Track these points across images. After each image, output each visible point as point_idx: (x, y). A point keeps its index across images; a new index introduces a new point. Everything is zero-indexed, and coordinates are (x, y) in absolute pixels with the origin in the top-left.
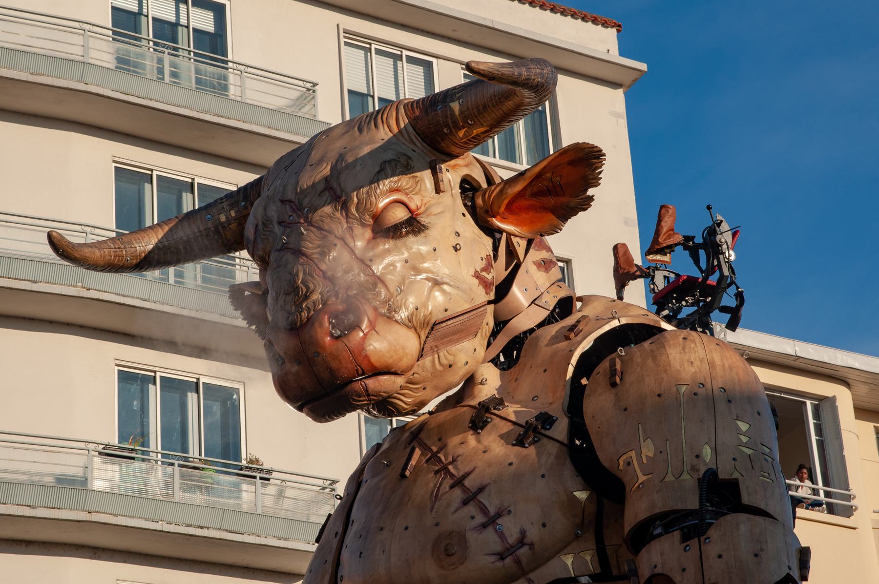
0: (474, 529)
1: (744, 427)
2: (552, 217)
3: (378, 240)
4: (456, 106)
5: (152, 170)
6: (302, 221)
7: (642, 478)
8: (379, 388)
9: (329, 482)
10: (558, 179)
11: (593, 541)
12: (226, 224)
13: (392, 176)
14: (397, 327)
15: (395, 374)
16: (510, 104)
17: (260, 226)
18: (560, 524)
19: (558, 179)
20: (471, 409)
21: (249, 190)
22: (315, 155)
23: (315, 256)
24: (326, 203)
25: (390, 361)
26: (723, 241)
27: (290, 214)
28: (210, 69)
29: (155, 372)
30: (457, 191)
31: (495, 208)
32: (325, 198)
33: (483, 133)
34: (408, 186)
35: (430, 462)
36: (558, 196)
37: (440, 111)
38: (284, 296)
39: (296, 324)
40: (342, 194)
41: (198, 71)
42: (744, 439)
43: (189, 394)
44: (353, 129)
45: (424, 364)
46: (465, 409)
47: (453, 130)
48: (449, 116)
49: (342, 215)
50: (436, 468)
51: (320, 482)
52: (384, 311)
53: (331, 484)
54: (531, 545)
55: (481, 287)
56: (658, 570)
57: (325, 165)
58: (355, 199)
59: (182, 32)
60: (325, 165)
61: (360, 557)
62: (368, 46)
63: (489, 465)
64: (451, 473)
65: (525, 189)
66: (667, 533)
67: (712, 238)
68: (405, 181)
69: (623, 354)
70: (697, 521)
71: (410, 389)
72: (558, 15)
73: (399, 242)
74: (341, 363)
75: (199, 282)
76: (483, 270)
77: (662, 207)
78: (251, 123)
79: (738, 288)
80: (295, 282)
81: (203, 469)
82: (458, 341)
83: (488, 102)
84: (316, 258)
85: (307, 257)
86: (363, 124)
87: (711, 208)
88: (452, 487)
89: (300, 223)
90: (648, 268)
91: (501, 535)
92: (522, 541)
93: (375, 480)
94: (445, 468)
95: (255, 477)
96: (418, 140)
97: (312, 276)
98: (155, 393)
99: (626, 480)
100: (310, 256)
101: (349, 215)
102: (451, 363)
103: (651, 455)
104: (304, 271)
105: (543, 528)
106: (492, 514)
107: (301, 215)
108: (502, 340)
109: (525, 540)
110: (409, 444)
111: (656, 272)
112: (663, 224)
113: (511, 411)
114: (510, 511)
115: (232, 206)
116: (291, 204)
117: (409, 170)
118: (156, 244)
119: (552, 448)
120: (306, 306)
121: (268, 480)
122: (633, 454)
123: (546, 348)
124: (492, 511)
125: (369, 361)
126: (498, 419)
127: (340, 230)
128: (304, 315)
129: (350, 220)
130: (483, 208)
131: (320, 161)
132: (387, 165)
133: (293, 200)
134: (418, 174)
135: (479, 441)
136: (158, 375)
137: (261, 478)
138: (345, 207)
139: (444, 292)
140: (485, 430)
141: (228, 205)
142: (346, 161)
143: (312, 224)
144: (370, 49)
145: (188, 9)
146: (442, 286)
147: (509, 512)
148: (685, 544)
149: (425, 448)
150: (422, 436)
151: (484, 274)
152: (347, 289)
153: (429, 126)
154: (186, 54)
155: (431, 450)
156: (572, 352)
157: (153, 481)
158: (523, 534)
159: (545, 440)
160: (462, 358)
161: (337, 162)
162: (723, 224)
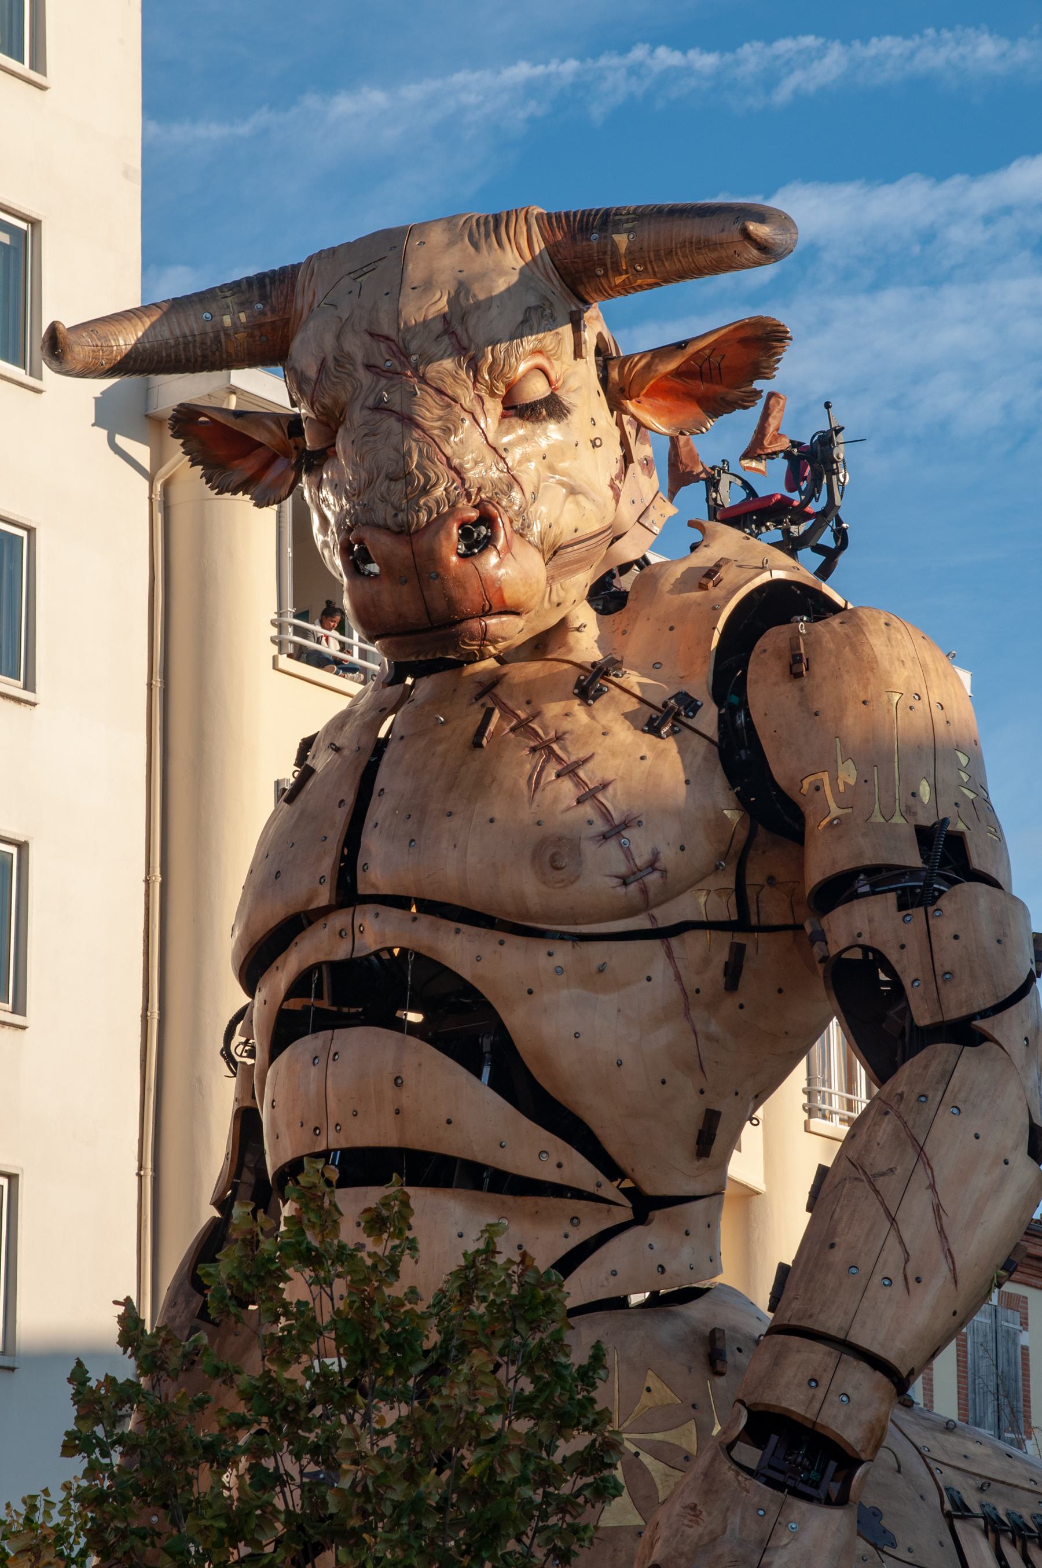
0: (592, 838)
2: (698, 410)
6: (409, 373)
7: (835, 811)
11: (733, 879)
12: (231, 332)
17: (330, 363)
20: (575, 668)
24: (445, 352)
25: (523, 598)
26: (841, 456)
27: (387, 357)
32: (443, 346)
34: (550, 348)
35: (518, 731)
36: (712, 382)
37: (595, 243)
38: (387, 481)
39: (409, 527)
40: (470, 346)
44: (462, 239)
46: (566, 666)
47: (610, 273)
48: (609, 253)
50: (532, 744)
54: (664, 872)
57: (438, 295)
58: (490, 357)
60: (438, 295)
64: (558, 756)
68: (548, 339)
69: (804, 631)
73: (538, 429)
74: (466, 593)
80: (406, 465)
82: (575, 571)
83: (676, 248)
84: (437, 435)
85: (423, 431)
87: (830, 407)
89: (406, 375)
90: (713, 468)
91: (628, 853)
92: (652, 865)
94: (546, 747)
96: (555, 275)
97: (433, 463)
99: (808, 810)
100: (428, 430)
101: (479, 377)
103: (852, 781)
104: (420, 451)
105: (681, 852)
106: (617, 822)
107: (407, 364)
109: (657, 865)
110: (477, 700)
111: (723, 475)
112: (771, 420)
113: (633, 679)
114: (640, 822)
115: (243, 305)
116: (391, 344)
119: (700, 746)
120: (425, 504)
123: (668, 597)
124: (617, 818)
126: (618, 691)
127: (468, 400)
128: (424, 517)
129: (478, 385)
130: (618, 384)
131: (428, 286)
135: (593, 718)
138: (474, 367)
139: (578, 503)
141: (236, 303)
142: (474, 296)
143: (425, 381)
146: (577, 496)
147: (640, 824)
148: (904, 913)
149: (508, 712)
150: (500, 691)
153: (576, 260)
155: (517, 716)
156: (716, 610)
158: (655, 857)
159: (687, 732)
161: (458, 293)
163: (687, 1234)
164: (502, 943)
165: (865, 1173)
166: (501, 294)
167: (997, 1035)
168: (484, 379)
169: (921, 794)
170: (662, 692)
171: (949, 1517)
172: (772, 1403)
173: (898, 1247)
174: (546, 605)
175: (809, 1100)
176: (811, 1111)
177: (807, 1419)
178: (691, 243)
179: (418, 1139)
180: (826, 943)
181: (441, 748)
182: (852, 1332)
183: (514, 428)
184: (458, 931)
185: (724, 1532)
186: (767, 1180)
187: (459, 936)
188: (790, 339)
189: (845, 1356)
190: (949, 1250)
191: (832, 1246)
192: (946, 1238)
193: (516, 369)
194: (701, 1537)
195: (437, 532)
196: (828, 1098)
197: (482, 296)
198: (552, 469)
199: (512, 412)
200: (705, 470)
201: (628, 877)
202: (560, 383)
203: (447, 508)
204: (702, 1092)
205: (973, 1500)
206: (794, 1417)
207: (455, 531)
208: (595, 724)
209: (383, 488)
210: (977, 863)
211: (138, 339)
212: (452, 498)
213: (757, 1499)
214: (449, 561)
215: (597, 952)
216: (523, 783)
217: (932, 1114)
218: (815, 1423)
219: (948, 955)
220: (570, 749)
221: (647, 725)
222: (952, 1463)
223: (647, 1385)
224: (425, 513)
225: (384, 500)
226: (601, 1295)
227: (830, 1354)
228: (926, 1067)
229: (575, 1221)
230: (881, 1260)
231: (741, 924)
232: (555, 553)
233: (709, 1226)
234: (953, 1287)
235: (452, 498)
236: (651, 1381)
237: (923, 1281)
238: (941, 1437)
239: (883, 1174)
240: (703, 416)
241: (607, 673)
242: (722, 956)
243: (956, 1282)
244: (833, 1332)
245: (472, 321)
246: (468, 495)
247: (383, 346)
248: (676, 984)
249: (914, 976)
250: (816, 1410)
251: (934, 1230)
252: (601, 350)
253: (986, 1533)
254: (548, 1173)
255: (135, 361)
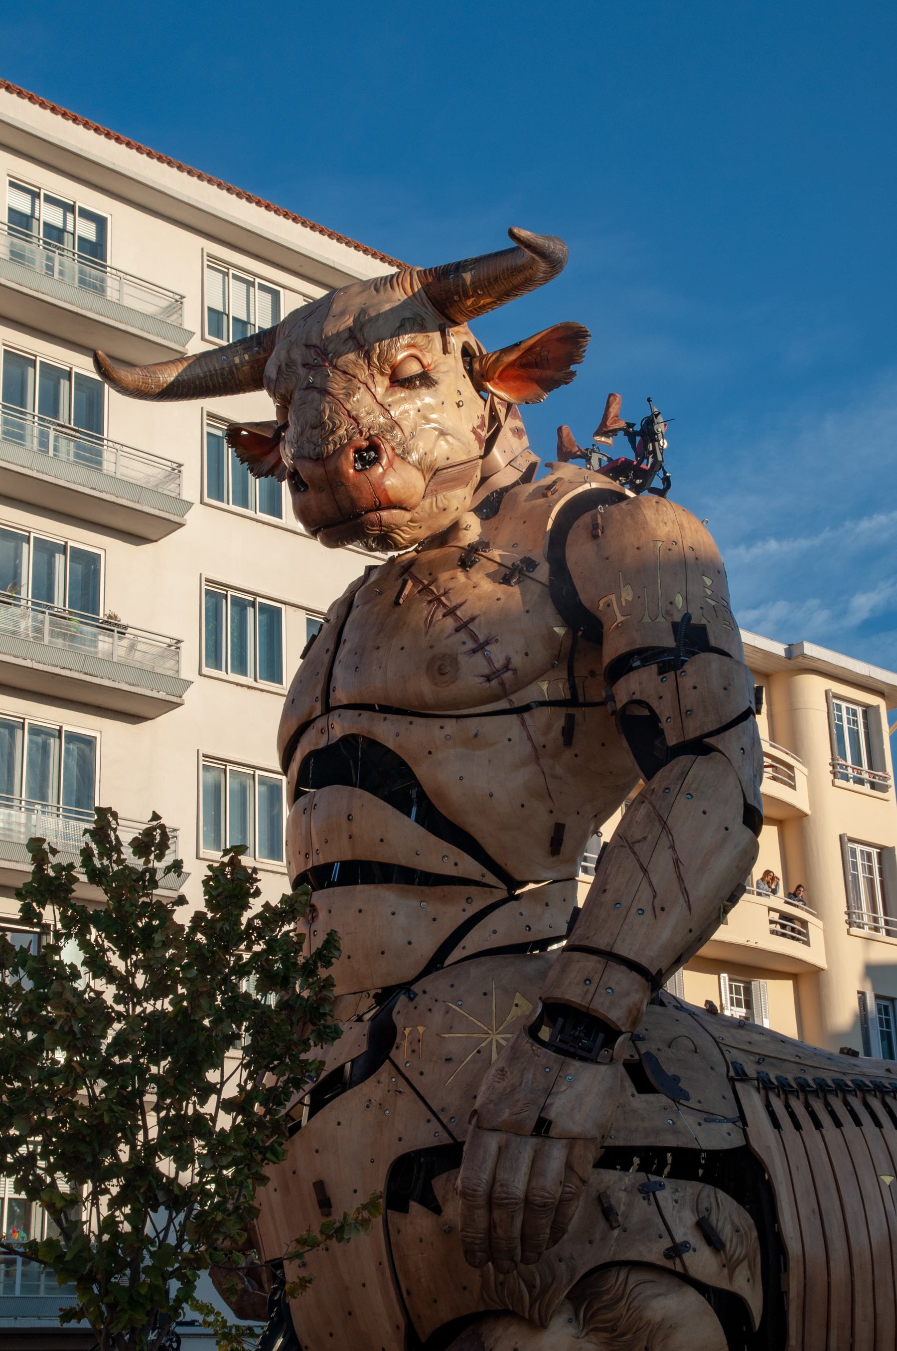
0: (465, 653)
1: (708, 582)
3: (396, 388)
4: (468, 277)
5: (36, 356)
6: (327, 364)
7: (620, 618)
8: (391, 521)
9: (175, 641)
10: (546, 353)
11: (566, 672)
12: (240, 366)
13: (410, 333)
14: (410, 467)
15: (405, 509)
16: (519, 278)
17: (284, 367)
18: (541, 654)
19: (546, 353)
21: (262, 338)
22: (336, 308)
23: (341, 396)
24: (350, 349)
25: (403, 497)
26: (660, 430)
27: (315, 357)
28: (94, 272)
29: (29, 532)
30: (459, 354)
31: (490, 374)
32: (349, 346)
33: (488, 304)
34: (422, 344)
37: (452, 280)
39: (323, 455)
41: (81, 272)
42: (709, 592)
43: (57, 555)
45: (424, 505)
46: (454, 549)
47: (463, 298)
49: (364, 362)
50: (429, 598)
51: (168, 641)
52: (398, 451)
53: (176, 643)
54: (515, 671)
55: (476, 442)
56: (637, 697)
57: (348, 317)
58: (378, 349)
59: (67, 238)
60: (348, 317)
61: (356, 671)
62: (226, 270)
63: (480, 598)
65: (515, 360)
66: (644, 666)
67: (650, 427)
68: (420, 338)
70: (673, 658)
71: (409, 527)
72: (386, 264)
73: (414, 393)
74: (362, 493)
75: (72, 458)
76: (479, 427)
77: (610, 395)
78: (126, 324)
79: (665, 473)
80: (322, 418)
81: (69, 619)
82: (453, 488)
85: (333, 396)
86: (379, 285)
88: (444, 616)
89: (325, 366)
90: (587, 450)
91: (489, 660)
92: (507, 667)
93: (367, 607)
94: (438, 599)
95: (113, 631)
97: (339, 414)
98: (28, 553)
99: (604, 620)
102: (446, 507)
103: (630, 598)
104: (331, 409)
106: (481, 641)
108: (483, 494)
109: (510, 666)
110: (400, 577)
111: (593, 454)
112: (611, 409)
113: (496, 553)
115: (246, 350)
116: (317, 349)
117: (423, 329)
118: (177, 377)
119: (536, 589)
120: (332, 440)
121: (124, 634)
122: (613, 597)
124: (482, 638)
125: (387, 494)
127: (363, 376)
128: (331, 447)
129: (371, 368)
130: (479, 372)
131: (343, 313)
132: (406, 322)
133: (318, 344)
134: (430, 334)
135: (468, 578)
136: (32, 535)
137: (118, 632)
138: (368, 357)
139: (447, 441)
140: (473, 569)
144: (228, 274)
145: (75, 218)
147: (497, 641)
148: (662, 676)
149: (417, 581)
150: (413, 569)
151: (479, 430)
152: (369, 429)
154: (70, 255)
155: (422, 583)
156: (550, 508)
157: (23, 625)
158: (508, 660)
159: (529, 581)
160: (455, 504)
161: (359, 315)
162: (659, 417)
163: (547, 905)
164: (411, 723)
165: (627, 841)
166: (386, 312)
167: (720, 747)
168: (375, 363)
169: (676, 602)
170: (515, 557)
171: (732, 1080)
172: (559, 997)
173: (649, 889)
174: (435, 509)
175: (849, 918)
176: (850, 923)
177: (583, 1006)
178: (507, 269)
179: (364, 853)
180: (615, 702)
181: (377, 609)
182: (616, 946)
183: (396, 392)
184: (385, 719)
185: (521, 1085)
186: (828, 962)
187: (386, 722)
188: (590, 336)
189: (610, 963)
190: (685, 888)
191: (605, 891)
192: (682, 880)
193: (396, 356)
194: (505, 1089)
195: (340, 456)
196: (860, 916)
197: (373, 314)
198: (428, 420)
199: (397, 384)
200: (580, 450)
201: (491, 675)
202: (432, 367)
203: (346, 441)
204: (551, 812)
205: (751, 1070)
206: (574, 1005)
207: (351, 455)
208: (469, 581)
209: (308, 434)
210: (713, 642)
211: (179, 374)
212: (350, 434)
213: (545, 1061)
214: (348, 473)
215: (473, 725)
216: (422, 623)
217: (673, 800)
218: (588, 1008)
219: (690, 699)
220: (452, 599)
221: (503, 579)
222: (739, 1047)
223: (516, 1002)
224: (332, 445)
225: (309, 441)
226: (487, 946)
227: (600, 962)
228: (671, 771)
229: (469, 900)
230: (637, 897)
231: (572, 702)
232: (435, 474)
233: (564, 900)
234: (688, 912)
235: (350, 434)
236: (518, 999)
237: (666, 909)
238: (734, 1031)
239: (639, 841)
240: (540, 391)
241: (477, 550)
242: (560, 723)
243: (690, 909)
244: (602, 947)
245: (366, 330)
246: (361, 433)
247: (312, 351)
248: (529, 743)
249: (668, 715)
250: (589, 999)
251: (674, 876)
252: (466, 352)
253: (758, 1090)
254: (448, 869)
255: (178, 387)
